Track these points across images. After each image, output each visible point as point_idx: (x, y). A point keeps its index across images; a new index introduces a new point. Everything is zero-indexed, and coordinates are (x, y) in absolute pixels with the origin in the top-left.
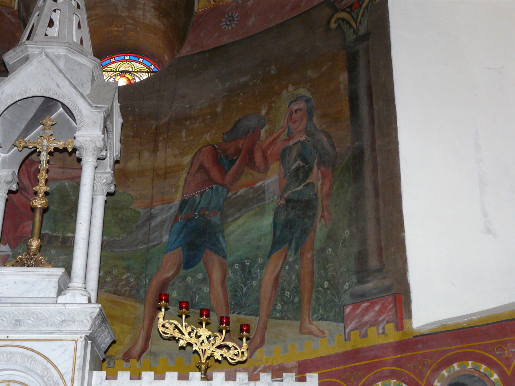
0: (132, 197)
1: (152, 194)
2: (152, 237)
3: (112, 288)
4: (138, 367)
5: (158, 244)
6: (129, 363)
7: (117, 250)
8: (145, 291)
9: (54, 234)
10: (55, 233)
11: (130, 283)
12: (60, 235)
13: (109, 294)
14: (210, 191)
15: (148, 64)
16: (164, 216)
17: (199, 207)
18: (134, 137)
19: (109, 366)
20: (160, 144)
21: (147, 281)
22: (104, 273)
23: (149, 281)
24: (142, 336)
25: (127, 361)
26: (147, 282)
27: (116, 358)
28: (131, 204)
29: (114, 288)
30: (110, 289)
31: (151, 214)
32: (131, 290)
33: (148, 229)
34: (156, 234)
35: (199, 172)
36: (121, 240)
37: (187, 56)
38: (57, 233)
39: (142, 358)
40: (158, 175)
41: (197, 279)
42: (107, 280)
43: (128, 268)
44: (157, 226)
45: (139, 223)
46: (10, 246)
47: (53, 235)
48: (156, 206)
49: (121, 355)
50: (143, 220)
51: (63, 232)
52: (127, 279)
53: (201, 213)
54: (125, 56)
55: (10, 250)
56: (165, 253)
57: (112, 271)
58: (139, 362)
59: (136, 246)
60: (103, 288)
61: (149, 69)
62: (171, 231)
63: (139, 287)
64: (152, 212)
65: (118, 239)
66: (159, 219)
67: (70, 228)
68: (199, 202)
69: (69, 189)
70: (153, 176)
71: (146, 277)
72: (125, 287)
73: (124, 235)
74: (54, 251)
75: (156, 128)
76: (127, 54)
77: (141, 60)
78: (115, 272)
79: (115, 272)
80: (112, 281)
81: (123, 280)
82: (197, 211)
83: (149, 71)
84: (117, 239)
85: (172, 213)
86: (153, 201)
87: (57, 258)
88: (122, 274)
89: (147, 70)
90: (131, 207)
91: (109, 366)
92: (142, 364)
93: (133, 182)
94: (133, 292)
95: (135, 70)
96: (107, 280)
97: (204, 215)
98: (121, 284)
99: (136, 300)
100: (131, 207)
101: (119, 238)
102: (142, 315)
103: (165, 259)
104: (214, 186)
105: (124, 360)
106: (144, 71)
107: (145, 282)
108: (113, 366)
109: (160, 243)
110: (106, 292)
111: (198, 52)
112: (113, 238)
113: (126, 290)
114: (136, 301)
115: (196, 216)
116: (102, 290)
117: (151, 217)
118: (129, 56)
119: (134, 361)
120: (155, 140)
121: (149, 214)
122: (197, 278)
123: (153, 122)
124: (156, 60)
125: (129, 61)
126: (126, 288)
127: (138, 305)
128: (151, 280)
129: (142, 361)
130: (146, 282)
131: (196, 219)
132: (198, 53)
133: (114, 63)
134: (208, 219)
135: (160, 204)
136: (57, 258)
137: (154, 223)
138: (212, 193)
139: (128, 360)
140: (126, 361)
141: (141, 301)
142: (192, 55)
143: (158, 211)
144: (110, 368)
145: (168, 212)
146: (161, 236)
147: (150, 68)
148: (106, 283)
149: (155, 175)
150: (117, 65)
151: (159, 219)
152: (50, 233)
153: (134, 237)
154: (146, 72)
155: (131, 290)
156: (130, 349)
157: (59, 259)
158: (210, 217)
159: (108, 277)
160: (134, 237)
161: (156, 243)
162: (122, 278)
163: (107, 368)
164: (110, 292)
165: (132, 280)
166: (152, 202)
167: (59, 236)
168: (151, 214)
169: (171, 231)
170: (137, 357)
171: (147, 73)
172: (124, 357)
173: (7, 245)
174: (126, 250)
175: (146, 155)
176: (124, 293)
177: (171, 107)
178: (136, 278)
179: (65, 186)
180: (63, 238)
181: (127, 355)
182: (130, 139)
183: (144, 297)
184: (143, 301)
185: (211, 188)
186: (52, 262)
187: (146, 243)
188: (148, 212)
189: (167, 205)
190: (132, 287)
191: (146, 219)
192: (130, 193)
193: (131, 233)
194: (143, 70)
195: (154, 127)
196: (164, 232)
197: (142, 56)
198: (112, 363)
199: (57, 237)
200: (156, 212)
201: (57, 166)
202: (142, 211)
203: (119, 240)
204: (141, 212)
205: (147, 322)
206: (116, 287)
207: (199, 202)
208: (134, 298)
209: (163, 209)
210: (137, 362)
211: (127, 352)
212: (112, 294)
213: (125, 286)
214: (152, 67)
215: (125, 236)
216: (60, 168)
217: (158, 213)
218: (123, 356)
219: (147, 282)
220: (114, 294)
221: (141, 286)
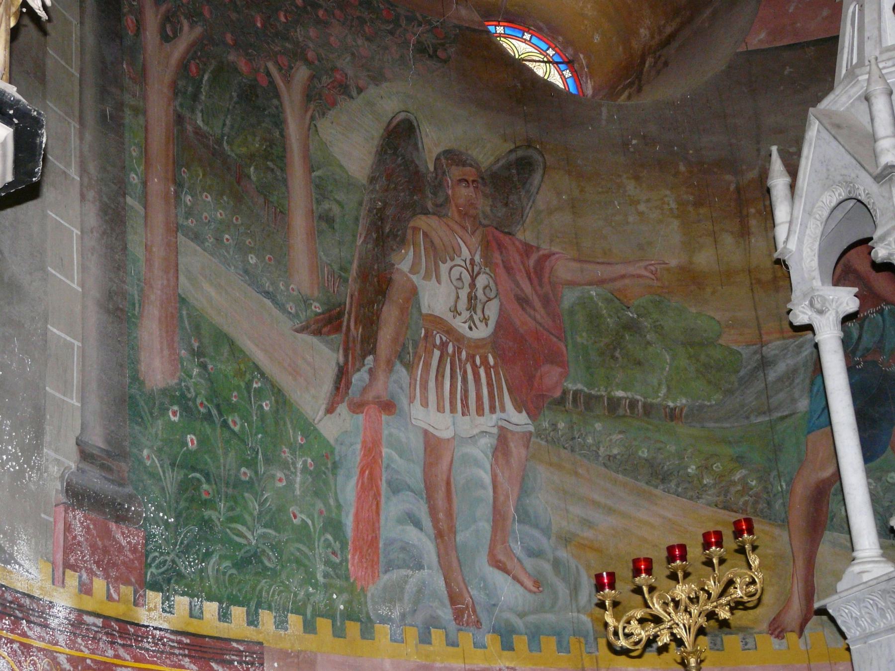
0: (718, 322)
1: (757, 318)
2: (774, 401)
3: (718, 498)
4: (803, 648)
5: (790, 415)
6: (784, 641)
7: (711, 425)
8: (784, 504)
9: (593, 392)
10: (593, 389)
11: (752, 489)
12: (604, 394)
13: (715, 509)
14: (879, 317)
15: (544, 46)
16: (791, 362)
17: (861, 347)
18: (698, 204)
19: (746, 647)
20: (753, 222)
21: (784, 484)
22: (696, 469)
23: (786, 485)
24: (796, 591)
25: (780, 636)
26: (784, 487)
27: (757, 630)
28: (719, 336)
29: (722, 498)
30: (715, 499)
31: (763, 357)
32: (756, 502)
33: (763, 385)
34: (781, 396)
35: (845, 280)
36: (716, 404)
37: (763, 50)
38: (596, 389)
39: (807, 632)
40: (759, 281)
41: (887, 484)
42: (705, 482)
43: (740, 460)
44: (780, 379)
45: (742, 373)
46: (528, 413)
47: (590, 394)
48: (770, 342)
49: (765, 626)
50: (749, 367)
51: (606, 388)
52: (743, 479)
53: (869, 358)
54: (496, 26)
55: (530, 422)
56: (809, 433)
57: (712, 465)
58: (803, 637)
59: (748, 418)
60: (701, 498)
61: (545, 56)
62: (811, 391)
63: (770, 496)
64: (764, 354)
65: (709, 404)
66: (781, 368)
67: (617, 380)
68: (860, 337)
69: (600, 304)
70: (751, 284)
71: (779, 477)
72: (742, 496)
73: (718, 396)
74: (600, 425)
75: (738, 190)
76: (499, 22)
77: (527, 36)
78: (717, 467)
79: (717, 467)
80: (714, 485)
81: (734, 483)
82: (859, 353)
83: (545, 59)
84: (706, 403)
85: (806, 356)
86: (762, 332)
87: (608, 439)
88: (731, 471)
89: (543, 57)
90: (720, 342)
91: (746, 647)
92: (809, 642)
93: (713, 293)
94: (760, 506)
95: (519, 56)
96: (705, 482)
97: (875, 363)
98: (733, 490)
99: (771, 522)
100: (720, 342)
101: (709, 401)
102: (789, 550)
103: (810, 444)
104: (886, 308)
105: (772, 634)
106: (537, 59)
107: (779, 488)
108: (754, 647)
109: (794, 414)
110: (709, 505)
111: (785, 44)
112: (700, 401)
113: (746, 503)
114: (770, 524)
115: (859, 364)
116: (701, 500)
117: (764, 364)
118: (504, 26)
119: (792, 637)
120: (741, 212)
121: (758, 356)
122: (888, 482)
123: (728, 177)
124: (561, 39)
125: (505, 38)
126: (747, 498)
127: (777, 531)
128: (791, 483)
129: (808, 638)
130: (781, 486)
131: (859, 369)
132: (789, 47)
133: (525, 42)
134: (886, 370)
135: (778, 339)
136: (608, 439)
137: (772, 376)
138: (884, 321)
139: (781, 635)
140: (777, 637)
141: (780, 523)
142: (777, 48)
143: (777, 352)
144: (749, 649)
145: (798, 353)
146: (794, 401)
147: (548, 54)
148: (704, 489)
149: (754, 282)
150: (527, 50)
151: (781, 368)
152: (586, 389)
153: (738, 400)
154: (539, 61)
155: (756, 502)
156: (779, 615)
157: (611, 440)
158: (890, 366)
159: (705, 476)
160: (738, 400)
161: (785, 414)
162: (733, 478)
163: (743, 650)
164: (716, 506)
165: (754, 483)
166: (761, 334)
167: (602, 396)
168: (763, 357)
169: (811, 391)
170: (797, 629)
171: (542, 64)
172: (772, 628)
173: (524, 413)
174: (728, 425)
175: (728, 240)
176: (744, 508)
177: (758, 150)
178: (760, 479)
179: (591, 298)
180: (608, 399)
181: (776, 626)
182: (691, 208)
183: (783, 515)
184: (785, 523)
185: (882, 312)
186: (601, 446)
187: (764, 413)
188: (755, 353)
189: (791, 340)
190: (757, 495)
191: (756, 367)
192: (712, 314)
193: (730, 392)
194: (534, 58)
195: (732, 187)
196: (797, 393)
197: (529, 29)
198: (750, 641)
199: (599, 398)
200: (773, 353)
201: (569, 257)
202: (745, 352)
203: (711, 406)
204: (742, 352)
205: (800, 563)
206: (725, 496)
207: (860, 337)
208: (764, 517)
209: (785, 348)
210: (800, 638)
211: (774, 619)
212: (722, 509)
213: (742, 493)
214: (551, 52)
215: (721, 397)
216: (574, 260)
217: (776, 355)
218: (770, 626)
219: (784, 487)
220: (725, 508)
221: (775, 495)
